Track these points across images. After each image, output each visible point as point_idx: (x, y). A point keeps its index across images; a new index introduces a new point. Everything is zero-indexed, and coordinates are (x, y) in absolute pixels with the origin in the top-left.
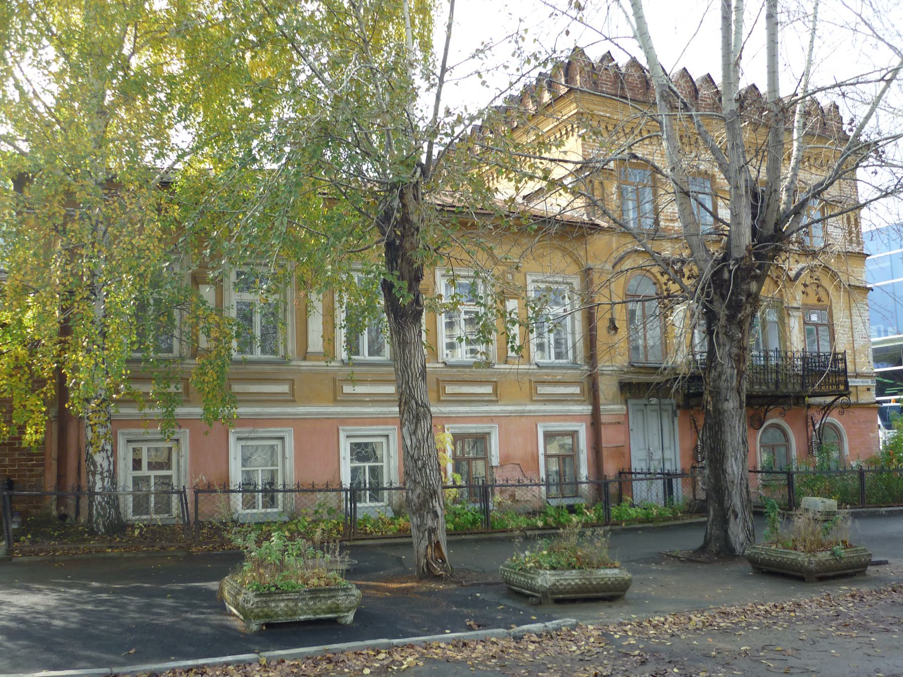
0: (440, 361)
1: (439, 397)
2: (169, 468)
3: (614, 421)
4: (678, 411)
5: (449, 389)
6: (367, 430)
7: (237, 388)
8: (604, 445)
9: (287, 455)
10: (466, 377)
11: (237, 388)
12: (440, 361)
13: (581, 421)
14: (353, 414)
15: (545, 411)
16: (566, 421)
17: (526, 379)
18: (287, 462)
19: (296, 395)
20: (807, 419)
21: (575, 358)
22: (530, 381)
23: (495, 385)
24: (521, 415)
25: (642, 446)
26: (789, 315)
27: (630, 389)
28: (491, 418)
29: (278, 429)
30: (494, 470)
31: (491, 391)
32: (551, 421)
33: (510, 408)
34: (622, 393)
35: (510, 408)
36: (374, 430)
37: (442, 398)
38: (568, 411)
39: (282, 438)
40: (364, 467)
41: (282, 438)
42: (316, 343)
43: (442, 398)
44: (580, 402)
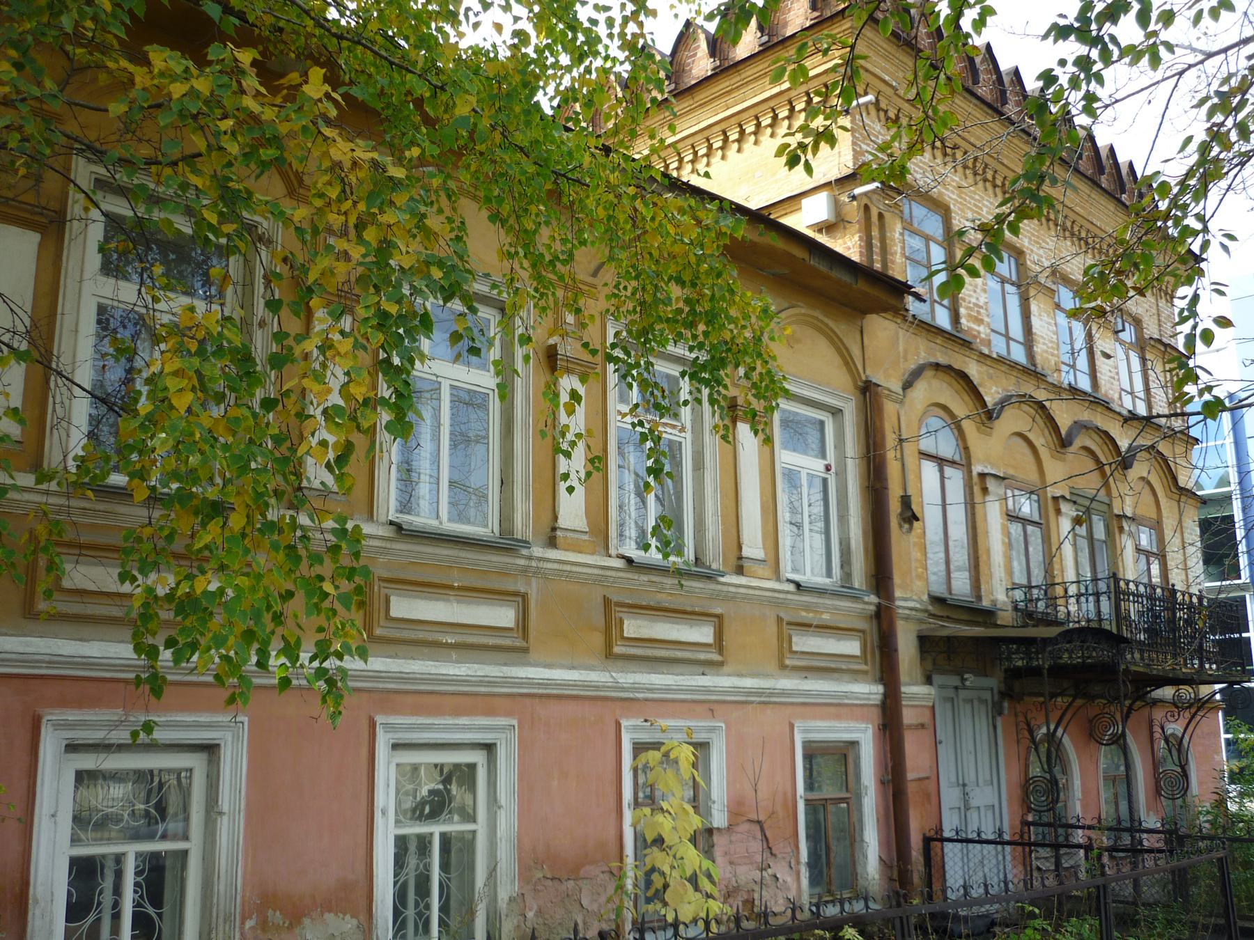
0: (383, 519)
1: (609, 645)
2: (186, 838)
3: (971, 724)
4: (1006, 704)
5: (633, 627)
6: (446, 728)
7: (404, 607)
8: (910, 775)
9: (225, 802)
10: (664, 599)
11: (404, 607)
12: (613, 552)
13: (864, 719)
14: (414, 680)
15: (807, 693)
16: (838, 717)
17: (771, 615)
18: (224, 825)
19: (532, 633)
20: (1151, 727)
21: (847, 576)
22: (780, 620)
23: (719, 622)
24: (767, 700)
25: (953, 779)
26: (1121, 529)
27: (939, 653)
28: (710, 705)
29: (204, 718)
30: (715, 838)
31: (709, 639)
32: (815, 718)
33: (749, 683)
34: (922, 659)
35: (749, 683)
36: (465, 728)
37: (617, 650)
38: (846, 695)
39: (210, 749)
40: (119, 859)
41: (210, 749)
42: (572, 510)
43: (617, 650)
44: (855, 675)
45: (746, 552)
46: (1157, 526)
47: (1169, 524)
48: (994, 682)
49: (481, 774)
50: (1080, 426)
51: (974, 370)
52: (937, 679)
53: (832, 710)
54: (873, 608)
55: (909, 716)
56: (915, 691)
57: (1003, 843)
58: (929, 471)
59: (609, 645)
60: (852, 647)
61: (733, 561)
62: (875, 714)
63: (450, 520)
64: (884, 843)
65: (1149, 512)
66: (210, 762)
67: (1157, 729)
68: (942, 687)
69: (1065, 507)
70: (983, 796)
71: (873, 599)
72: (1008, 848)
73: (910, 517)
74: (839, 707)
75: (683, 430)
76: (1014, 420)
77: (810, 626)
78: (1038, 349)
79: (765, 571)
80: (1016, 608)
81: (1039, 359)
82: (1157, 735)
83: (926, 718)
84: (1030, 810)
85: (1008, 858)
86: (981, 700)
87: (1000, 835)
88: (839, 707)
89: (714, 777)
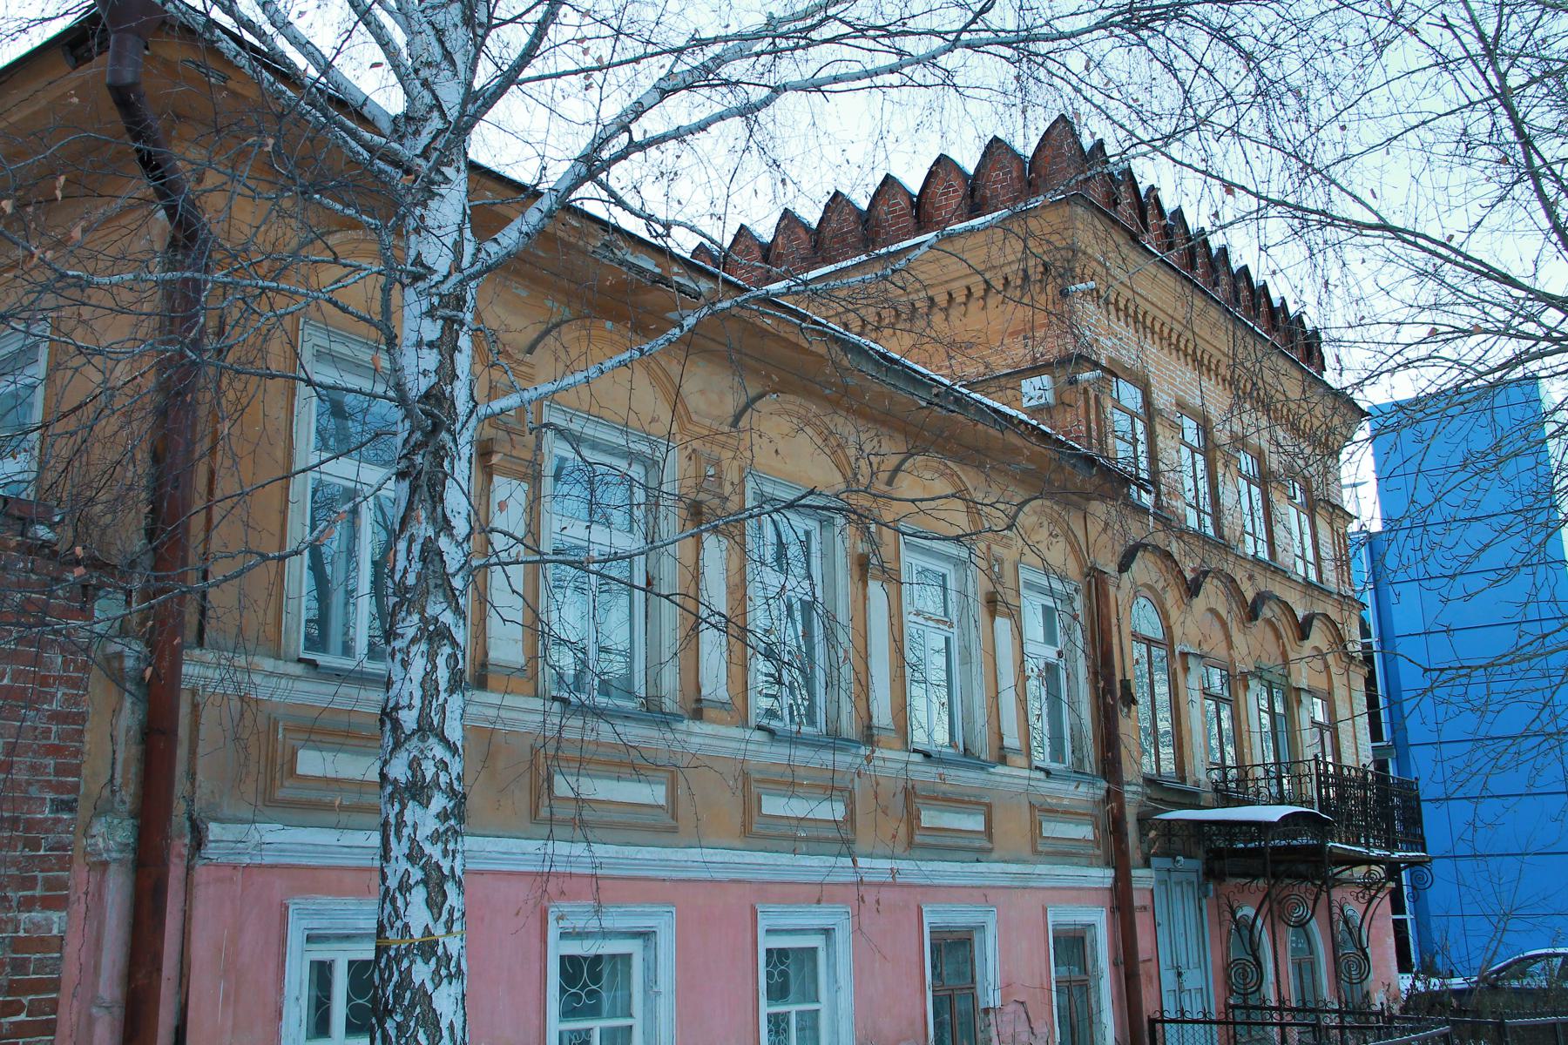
31: (982, 828)
43: (918, 839)
45: (1007, 742)
46: (1329, 699)
47: (1340, 694)
48: (1197, 864)
49: (822, 956)
50: (1262, 598)
51: (1175, 548)
52: (1154, 861)
53: (1074, 893)
54: (1103, 792)
55: (1138, 900)
56: (1143, 878)
57: (1211, 1022)
58: (1139, 651)
59: (910, 835)
60: (1085, 831)
61: (995, 752)
62: (1107, 897)
63: (306, 649)
64: (1119, 1025)
65: (1321, 683)
66: (645, 947)
67: (1336, 910)
68: (1158, 870)
69: (1253, 683)
70: (1193, 979)
71: (1105, 784)
72: (1215, 1027)
73: (1130, 700)
74: (1078, 893)
75: (951, 626)
76: (1212, 595)
77: (963, 802)
78: (1227, 521)
79: (1023, 761)
80: (1216, 790)
81: (1226, 532)
82: (1336, 917)
83: (1147, 902)
84: (1231, 992)
85: (1216, 1037)
86: (1190, 883)
87: (1183, 1014)
88: (1078, 893)
89: (661, 957)
